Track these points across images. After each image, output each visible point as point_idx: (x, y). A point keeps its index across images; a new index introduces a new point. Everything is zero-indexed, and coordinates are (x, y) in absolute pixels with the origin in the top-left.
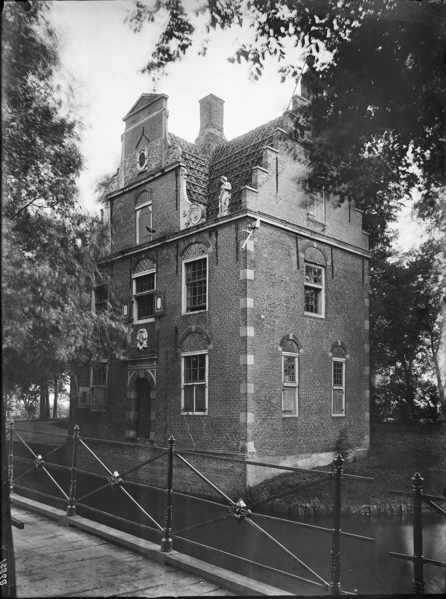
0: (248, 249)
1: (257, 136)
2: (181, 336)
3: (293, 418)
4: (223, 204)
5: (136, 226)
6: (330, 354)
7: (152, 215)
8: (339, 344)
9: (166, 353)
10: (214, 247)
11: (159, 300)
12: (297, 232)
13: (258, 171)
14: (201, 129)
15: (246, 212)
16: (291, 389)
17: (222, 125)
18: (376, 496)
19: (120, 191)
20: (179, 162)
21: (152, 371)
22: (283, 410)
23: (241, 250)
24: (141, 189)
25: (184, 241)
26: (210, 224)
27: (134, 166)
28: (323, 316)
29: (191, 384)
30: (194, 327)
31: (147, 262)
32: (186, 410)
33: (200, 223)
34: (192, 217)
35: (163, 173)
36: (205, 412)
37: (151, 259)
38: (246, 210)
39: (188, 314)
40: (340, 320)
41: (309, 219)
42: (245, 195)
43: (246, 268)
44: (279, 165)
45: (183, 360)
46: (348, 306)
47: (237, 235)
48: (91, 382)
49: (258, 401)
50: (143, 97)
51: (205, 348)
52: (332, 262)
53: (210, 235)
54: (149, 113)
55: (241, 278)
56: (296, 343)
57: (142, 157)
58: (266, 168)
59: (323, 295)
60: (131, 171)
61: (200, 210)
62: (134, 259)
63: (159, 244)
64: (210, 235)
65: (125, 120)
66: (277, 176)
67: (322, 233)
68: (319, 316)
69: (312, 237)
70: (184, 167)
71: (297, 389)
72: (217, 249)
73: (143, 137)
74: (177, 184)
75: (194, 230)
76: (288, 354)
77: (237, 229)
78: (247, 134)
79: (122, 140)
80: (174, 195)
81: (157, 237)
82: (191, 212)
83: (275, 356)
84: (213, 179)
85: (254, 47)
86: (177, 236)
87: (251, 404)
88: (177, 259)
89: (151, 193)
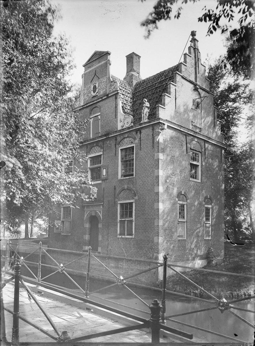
0: (160, 141)
1: (161, 77)
2: (117, 191)
3: (183, 240)
4: (145, 115)
5: (90, 127)
6: (204, 203)
7: (101, 121)
8: (209, 197)
9: (109, 201)
10: (139, 140)
11: (104, 170)
12: (186, 132)
13: (166, 96)
14: (127, 72)
15: (159, 120)
16: (182, 223)
17: (139, 70)
18: (235, 287)
19: (81, 107)
20: (118, 91)
21: (99, 212)
23: (155, 141)
24: (94, 106)
25: (120, 136)
26: (137, 127)
27: (90, 92)
28: (199, 181)
30: (126, 187)
31: (97, 148)
32: (120, 234)
33: (130, 126)
34: (126, 123)
35: (107, 96)
36: (132, 236)
37: (99, 146)
38: (159, 119)
39: (122, 178)
40: (209, 183)
42: (159, 110)
43: (159, 152)
44: (177, 93)
45: (119, 205)
46: (213, 175)
47: (153, 133)
48: (62, 218)
49: (165, 230)
50: (95, 53)
51: (133, 199)
52: (205, 150)
53: (137, 133)
54: (99, 62)
55: (156, 158)
56: (185, 196)
57: (95, 88)
58: (170, 94)
59: (200, 168)
60: (87, 96)
61: (130, 118)
62: (89, 146)
63: (105, 138)
64: (137, 133)
65: (84, 66)
66: (176, 99)
67: (200, 133)
68: (198, 181)
69: (194, 135)
70: (121, 93)
71: (186, 223)
72: (140, 141)
74: (116, 103)
75: (126, 130)
76: (181, 202)
77: (153, 129)
78: (155, 75)
79: (82, 77)
80: (114, 110)
81: (104, 134)
82: (124, 120)
83: (174, 204)
84: (136, 101)
85: (214, 13)
86: (116, 133)
87: (161, 232)
88: (116, 147)
89: (100, 108)
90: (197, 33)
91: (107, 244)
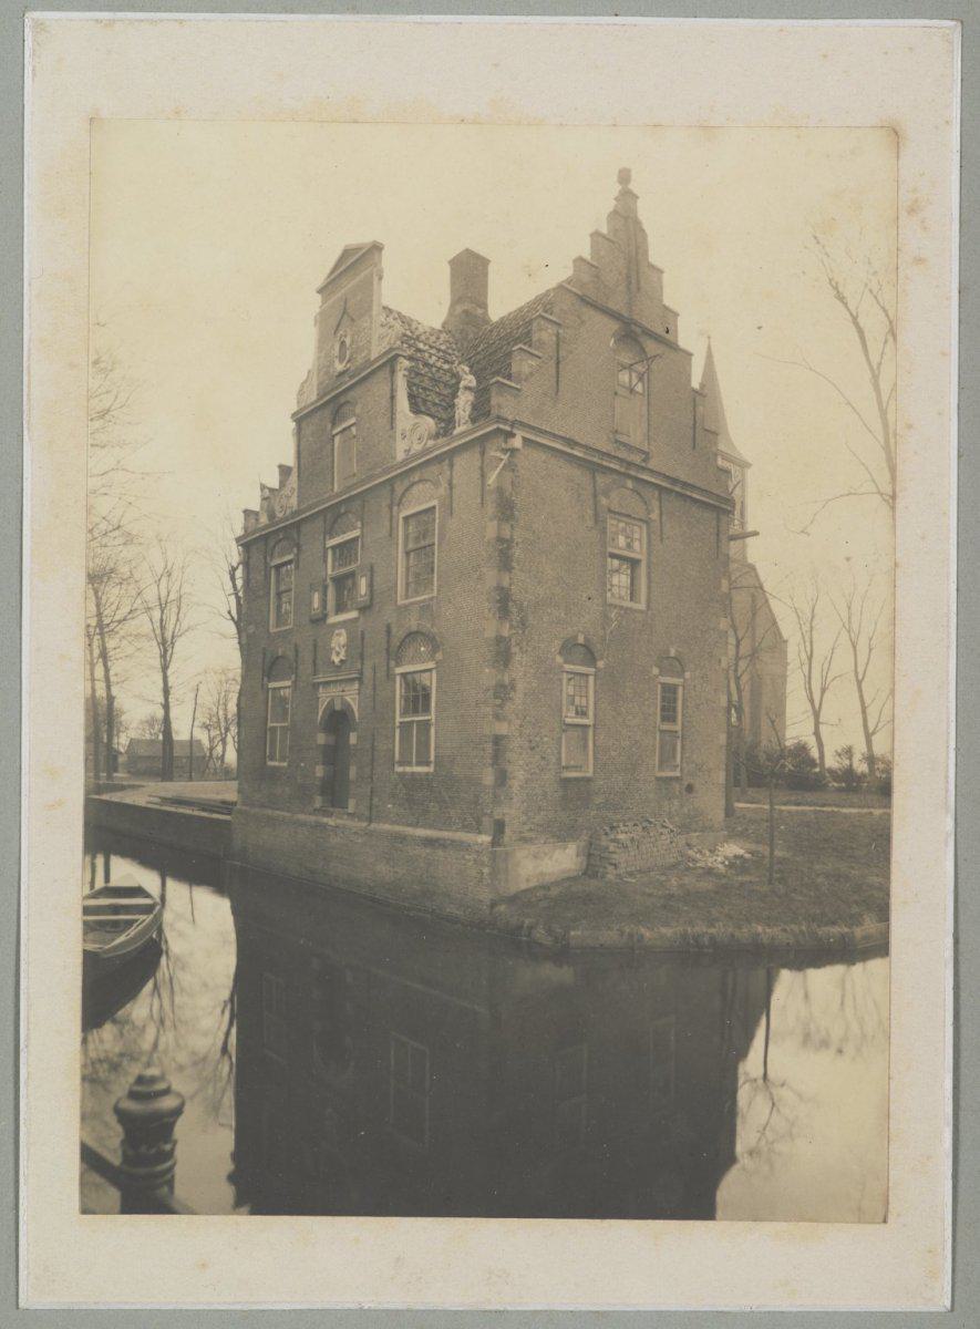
3: (583, 779)
6: (655, 671)
17: (486, 298)
22: (563, 764)
24: (342, 400)
27: (331, 363)
29: (409, 719)
32: (401, 763)
41: (616, 441)
47: (483, 463)
62: (329, 516)
65: (319, 292)
66: (558, 363)
71: (434, 672)
72: (451, 489)
73: (346, 316)
77: (483, 453)
90: (634, 175)
91: (369, 790)
